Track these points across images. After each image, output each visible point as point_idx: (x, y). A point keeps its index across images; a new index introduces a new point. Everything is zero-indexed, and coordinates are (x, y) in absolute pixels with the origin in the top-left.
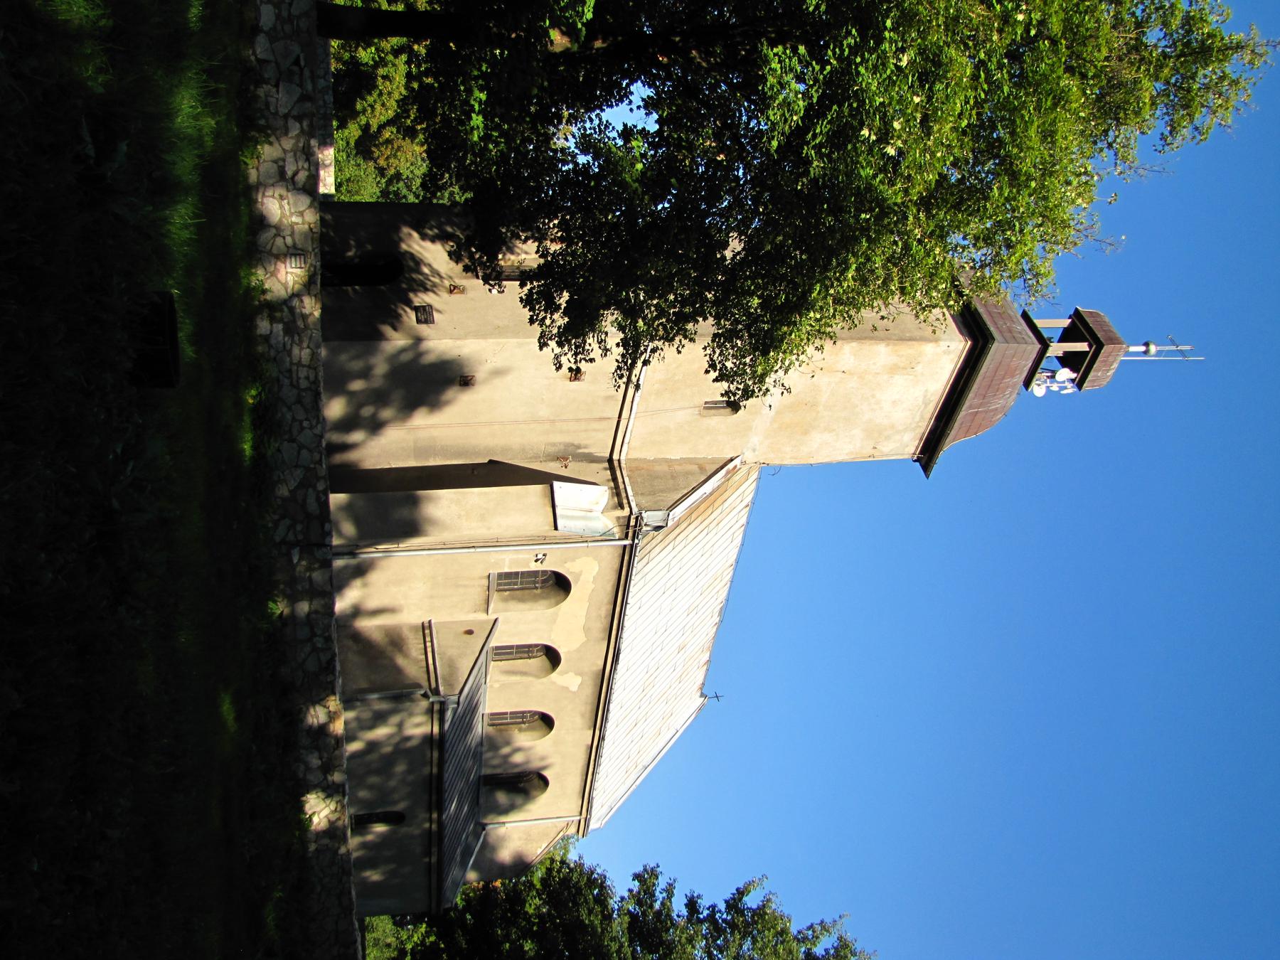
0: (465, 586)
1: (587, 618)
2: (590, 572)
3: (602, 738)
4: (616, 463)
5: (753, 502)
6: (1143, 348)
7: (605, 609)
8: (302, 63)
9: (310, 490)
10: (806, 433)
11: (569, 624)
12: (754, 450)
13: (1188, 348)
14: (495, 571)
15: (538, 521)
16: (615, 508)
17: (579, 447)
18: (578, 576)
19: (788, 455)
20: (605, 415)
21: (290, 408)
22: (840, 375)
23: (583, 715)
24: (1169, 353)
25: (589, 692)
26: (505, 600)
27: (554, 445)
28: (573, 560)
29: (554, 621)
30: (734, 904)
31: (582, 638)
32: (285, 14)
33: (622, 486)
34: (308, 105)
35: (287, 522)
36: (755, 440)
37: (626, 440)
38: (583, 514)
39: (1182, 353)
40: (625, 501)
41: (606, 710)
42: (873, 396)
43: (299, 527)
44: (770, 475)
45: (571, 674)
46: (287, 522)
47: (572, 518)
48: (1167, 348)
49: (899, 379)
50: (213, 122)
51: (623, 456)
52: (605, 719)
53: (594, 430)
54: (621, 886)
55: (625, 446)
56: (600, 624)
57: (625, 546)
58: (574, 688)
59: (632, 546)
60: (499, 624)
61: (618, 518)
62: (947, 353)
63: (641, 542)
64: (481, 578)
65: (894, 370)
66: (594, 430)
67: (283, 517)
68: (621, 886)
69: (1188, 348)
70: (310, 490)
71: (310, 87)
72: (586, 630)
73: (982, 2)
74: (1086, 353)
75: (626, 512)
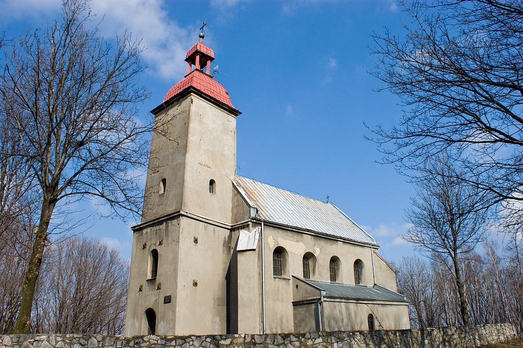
2: (273, 239)
3: (341, 238)
7: (290, 234)
11: (296, 248)
15: (253, 256)
17: (225, 241)
19: (232, 163)
27: (223, 251)
29: (293, 253)
41: (330, 235)
42: (211, 130)
44: (240, 171)
49: (205, 121)
52: (333, 236)
53: (219, 235)
56: (296, 237)
57: (264, 225)
60: (294, 275)
64: (275, 281)
65: (201, 122)
66: (219, 235)
72: (298, 241)
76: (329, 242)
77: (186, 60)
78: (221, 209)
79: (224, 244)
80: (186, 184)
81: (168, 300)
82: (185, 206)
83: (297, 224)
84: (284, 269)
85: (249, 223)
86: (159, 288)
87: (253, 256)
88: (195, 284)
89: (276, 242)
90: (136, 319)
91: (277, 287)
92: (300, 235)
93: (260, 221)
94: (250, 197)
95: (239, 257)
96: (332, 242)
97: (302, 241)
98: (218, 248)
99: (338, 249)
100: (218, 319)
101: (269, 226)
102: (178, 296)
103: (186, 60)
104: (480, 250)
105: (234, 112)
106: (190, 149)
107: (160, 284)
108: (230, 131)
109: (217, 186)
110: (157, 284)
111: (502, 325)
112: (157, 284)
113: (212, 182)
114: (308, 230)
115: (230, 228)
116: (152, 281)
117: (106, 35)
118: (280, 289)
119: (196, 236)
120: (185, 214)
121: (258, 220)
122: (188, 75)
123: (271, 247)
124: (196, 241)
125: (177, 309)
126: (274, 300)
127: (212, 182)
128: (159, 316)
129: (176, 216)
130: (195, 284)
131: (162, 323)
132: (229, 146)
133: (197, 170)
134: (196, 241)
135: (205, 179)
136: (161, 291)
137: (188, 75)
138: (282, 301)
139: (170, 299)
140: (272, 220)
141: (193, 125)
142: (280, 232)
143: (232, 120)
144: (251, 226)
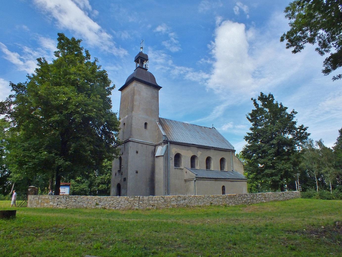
2: (174, 150)
3: (213, 147)
4: (156, 145)
7: (183, 147)
8: (58, 198)
9: (129, 199)
12: (155, 120)
14: (174, 167)
15: (162, 159)
16: (162, 145)
17: (152, 152)
18: (176, 152)
21: (114, 202)
25: (202, 150)
26: (181, 165)
27: (151, 156)
30: (251, 121)
32: (51, 200)
33: (159, 144)
34: (64, 197)
35: (134, 204)
37: (152, 143)
40: (161, 143)
42: (145, 98)
43: (136, 202)
46: (134, 204)
51: (130, 144)
55: (153, 143)
56: (187, 148)
57: (170, 143)
58: (201, 153)
60: (186, 167)
63: (169, 140)
67: (133, 204)
70: (129, 199)
71: (62, 197)
72: (188, 150)
73: (340, 52)
74: (141, 59)
75: (163, 143)
79: (152, 153)
80: (133, 126)
81: (125, 179)
84: (181, 164)
86: (122, 174)
87: (162, 159)
88: (137, 172)
93: (167, 141)
95: (157, 160)
100: (148, 188)
101: (173, 144)
102: (128, 178)
104: (337, 52)
107: (122, 172)
109: (148, 126)
110: (121, 172)
111: (308, 182)
113: (146, 124)
114: (193, 144)
115: (154, 145)
116: (119, 171)
117: (151, 87)
119: (137, 150)
123: (173, 154)
124: (137, 152)
127: (146, 124)
128: (122, 187)
129: (127, 141)
130: (137, 172)
134: (137, 152)
136: (123, 175)
140: (175, 140)
142: (178, 146)
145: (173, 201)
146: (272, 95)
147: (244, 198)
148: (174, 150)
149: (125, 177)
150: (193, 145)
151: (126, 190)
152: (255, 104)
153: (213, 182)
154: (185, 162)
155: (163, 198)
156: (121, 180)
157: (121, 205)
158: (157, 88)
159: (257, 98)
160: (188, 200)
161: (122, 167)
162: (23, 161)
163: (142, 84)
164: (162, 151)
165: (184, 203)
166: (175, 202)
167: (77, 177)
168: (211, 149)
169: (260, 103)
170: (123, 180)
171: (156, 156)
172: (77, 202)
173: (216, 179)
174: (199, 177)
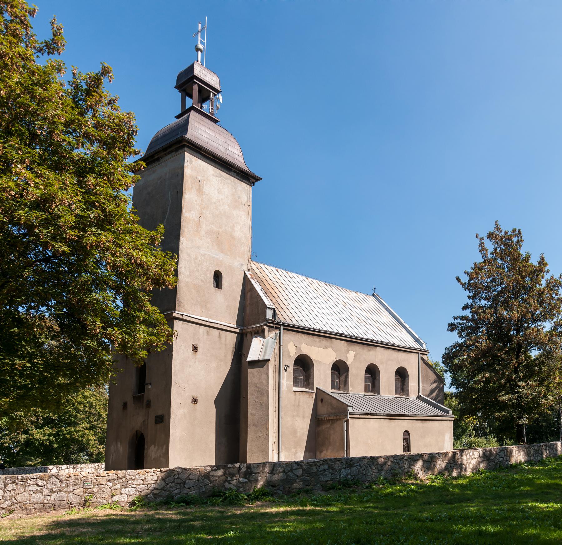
0: (299, 402)
1: (320, 347)
2: (294, 346)
3: (381, 343)
5: (276, 267)
6: (199, 52)
7: (317, 339)
10: (233, 238)
11: (323, 357)
12: (242, 265)
13: (200, 25)
19: (246, 247)
20: (218, 335)
21: (168, 484)
22: (201, 219)
23: (369, 351)
24: (203, 37)
25: (357, 348)
28: (289, 352)
29: (320, 362)
31: (330, 350)
36: (236, 264)
38: (264, 348)
39: (203, 29)
41: (367, 340)
42: (215, 203)
44: (255, 256)
45: (348, 355)
47: (265, 352)
48: (199, 38)
49: (206, 189)
50: (484, 344)
52: (371, 341)
53: (226, 341)
54: (454, 338)
55: (210, 320)
56: (324, 342)
57: (284, 329)
59: (284, 326)
61: (269, 331)
62: (191, 162)
64: (295, 395)
65: (200, 191)
66: (226, 341)
68: (454, 338)
69: (200, 25)
72: (326, 347)
76: (366, 348)
77: (175, 87)
78: (224, 309)
82: (180, 305)
83: (316, 324)
85: (265, 327)
88: (195, 401)
89: (298, 348)
90: (119, 443)
91: (297, 402)
92: (329, 340)
94: (266, 294)
96: (369, 347)
97: (331, 347)
98: (225, 356)
99: (376, 357)
103: (175, 87)
105: (247, 177)
106: (186, 230)
108: (242, 203)
109: (225, 282)
110: (145, 401)
112: (145, 401)
118: (301, 404)
119: (195, 344)
120: (180, 316)
121: (276, 324)
122: (401, 324)
123: (292, 355)
124: (195, 349)
125: (171, 431)
126: (294, 416)
128: (148, 439)
130: (195, 401)
131: (152, 447)
132: (242, 225)
133: (196, 259)
134: (195, 349)
135: (207, 270)
137: (401, 324)
138: (304, 417)
139: (156, 420)
141: (189, 197)
142: (304, 336)
143: (244, 190)
144: (266, 331)
145: (325, 470)
146: (520, 232)
147: (472, 459)
148: (294, 346)
149: (160, 413)
150: (339, 337)
151: (165, 447)
152: (483, 250)
153: (385, 423)
154: (387, 380)
155: (299, 466)
156: (144, 421)
157: (189, 489)
158: (249, 180)
159: (485, 235)
160: (359, 467)
161: (150, 387)
162: (92, 135)
163: (208, 161)
164: (266, 347)
165: (350, 474)
166: (329, 473)
167: (107, 413)
168: (378, 348)
169: (490, 246)
170: (152, 420)
171: (249, 359)
172: (46, 492)
173: (391, 417)
174: (356, 411)
